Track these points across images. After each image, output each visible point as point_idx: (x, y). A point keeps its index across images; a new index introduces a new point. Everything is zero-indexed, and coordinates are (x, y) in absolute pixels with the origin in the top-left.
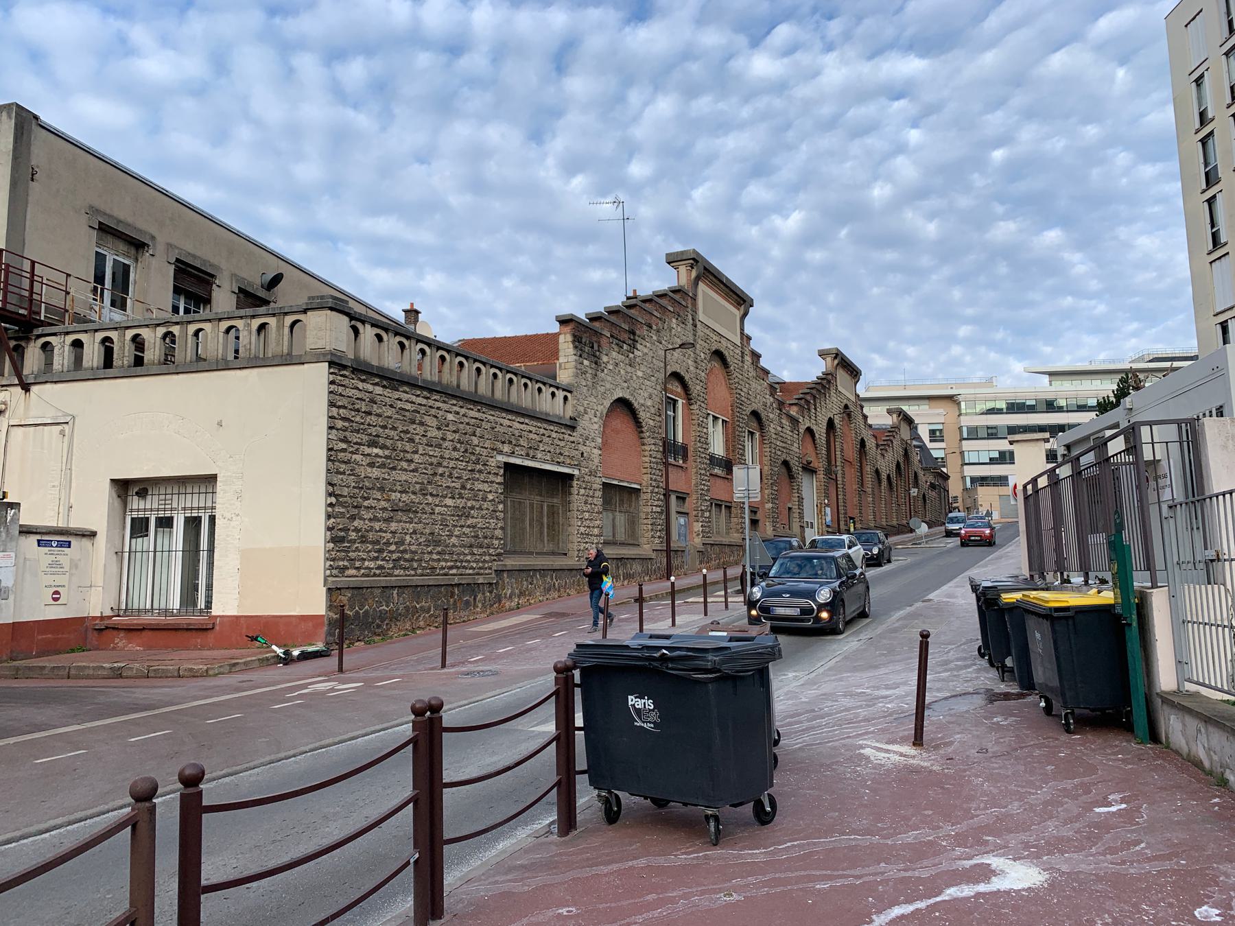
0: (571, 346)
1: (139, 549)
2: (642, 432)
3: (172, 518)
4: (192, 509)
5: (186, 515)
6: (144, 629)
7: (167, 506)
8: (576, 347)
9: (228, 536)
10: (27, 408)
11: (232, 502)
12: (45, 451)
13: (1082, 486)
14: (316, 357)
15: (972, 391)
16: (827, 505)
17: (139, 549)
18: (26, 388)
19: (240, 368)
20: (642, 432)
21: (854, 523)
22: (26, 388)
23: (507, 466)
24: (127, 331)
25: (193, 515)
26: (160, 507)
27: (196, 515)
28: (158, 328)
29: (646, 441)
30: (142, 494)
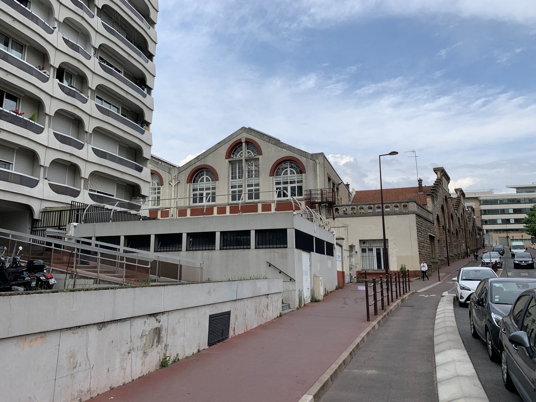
0: (431, 201)
1: (365, 255)
2: (440, 223)
4: (378, 246)
6: (373, 274)
8: (432, 202)
10: (334, 223)
13: (187, 186)
14: (413, 213)
15: (485, 195)
16: (464, 243)
18: (334, 219)
20: (440, 223)
21: (469, 248)
22: (334, 219)
23: (430, 235)
29: (440, 226)
30: (364, 243)
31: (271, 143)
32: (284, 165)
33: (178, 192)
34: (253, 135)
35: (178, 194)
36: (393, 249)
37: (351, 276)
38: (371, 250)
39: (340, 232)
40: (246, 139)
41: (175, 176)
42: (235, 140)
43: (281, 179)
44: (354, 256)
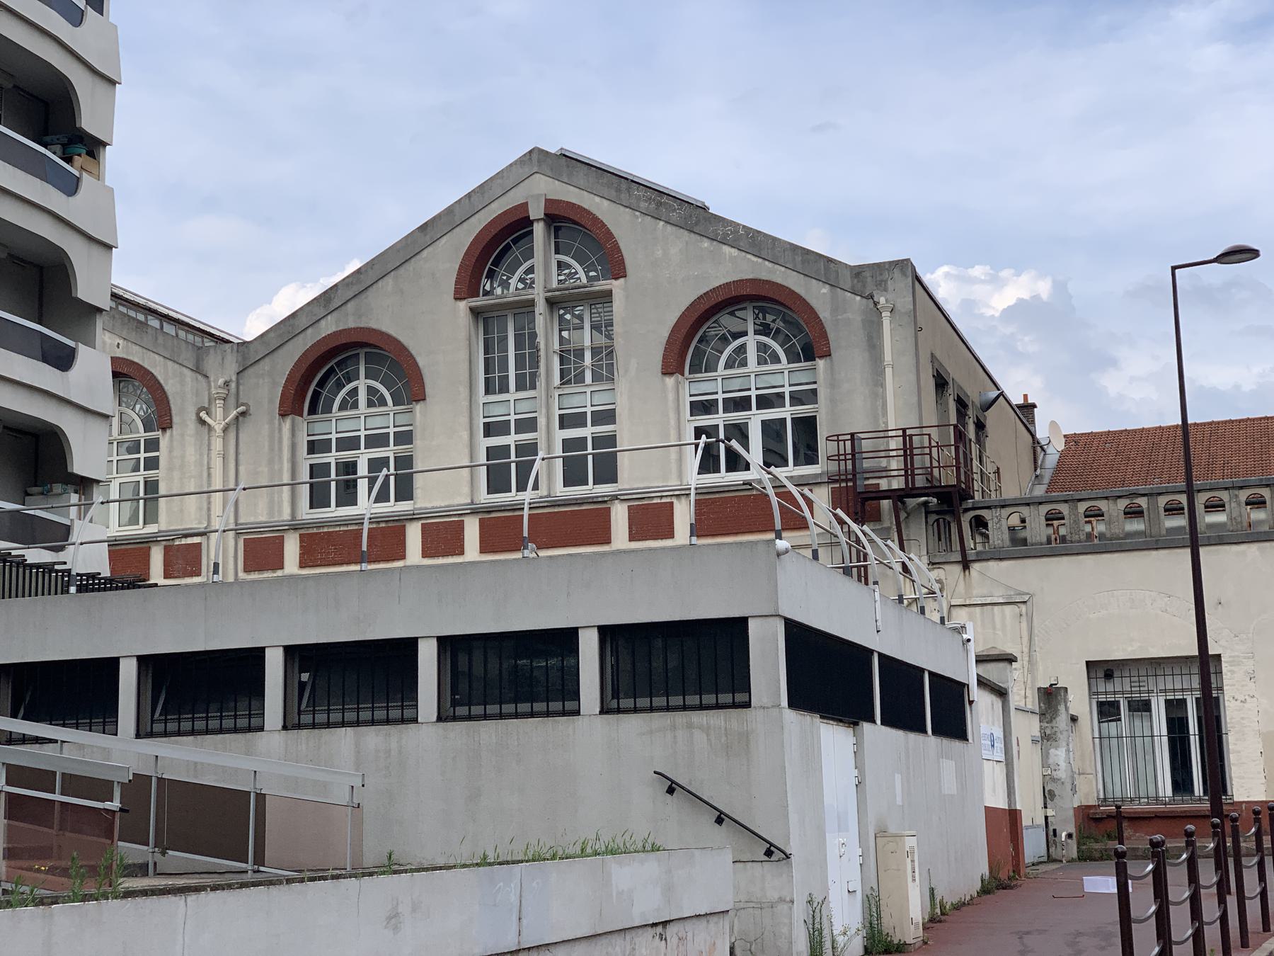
1: (1113, 733)
3: (1150, 701)
4: (1174, 691)
5: (1168, 698)
7: (1142, 689)
9: (1242, 718)
10: (968, 586)
11: (1244, 683)
12: (999, 633)
13: (280, 430)
17: (1113, 733)
18: (966, 564)
19: (1235, 543)
22: (966, 564)
24: (1079, 504)
25: (1176, 697)
26: (1133, 689)
27: (1181, 697)
28: (1118, 500)
30: (1109, 676)
31: (666, 222)
32: (728, 322)
33: (241, 456)
34: (582, 183)
35: (241, 468)
36: (1244, 702)
37: (1051, 828)
38: (1143, 707)
39: (994, 628)
40: (550, 203)
41: (227, 384)
42: (497, 209)
43: (716, 384)
44: (1062, 738)
